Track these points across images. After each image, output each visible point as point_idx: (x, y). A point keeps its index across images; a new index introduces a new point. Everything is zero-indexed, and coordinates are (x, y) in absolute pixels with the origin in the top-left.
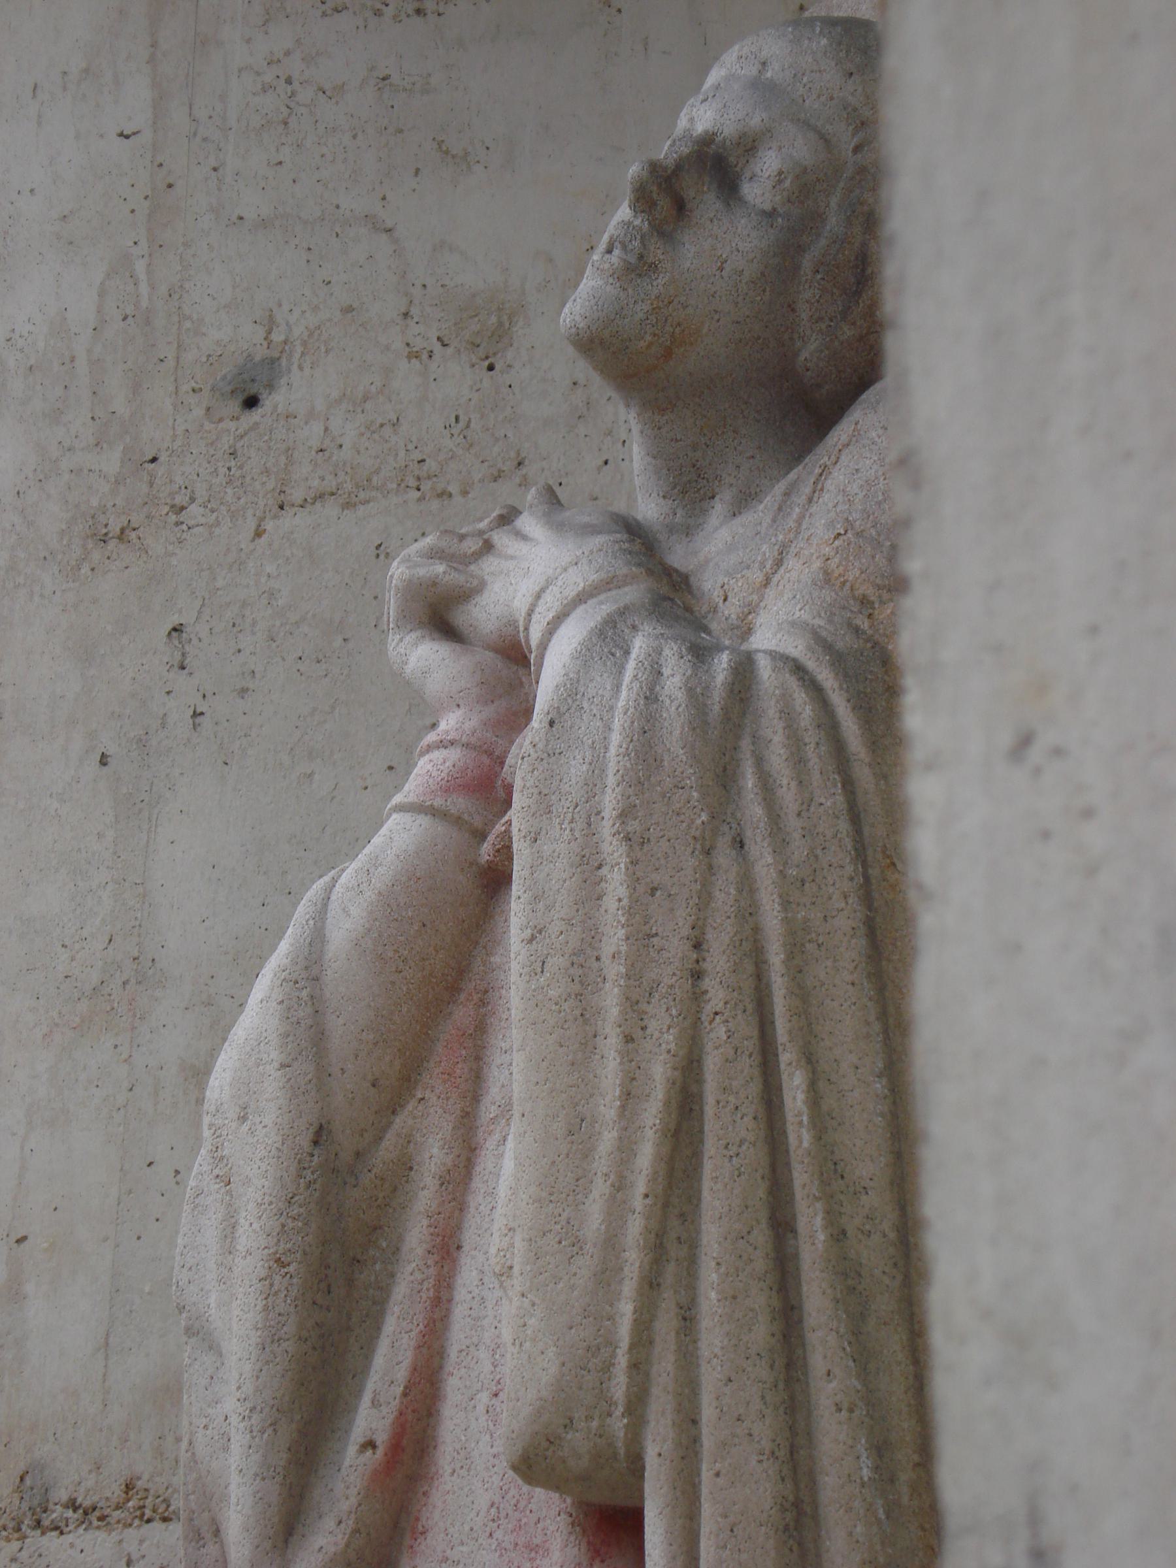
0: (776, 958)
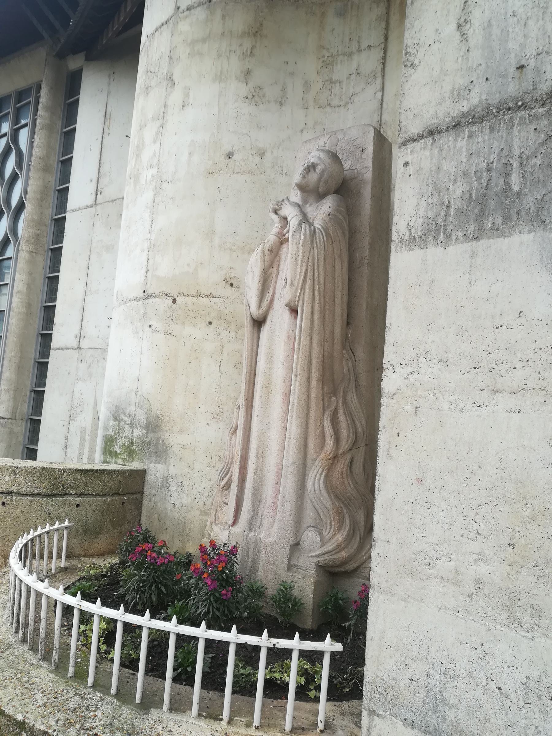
0: (316, 261)
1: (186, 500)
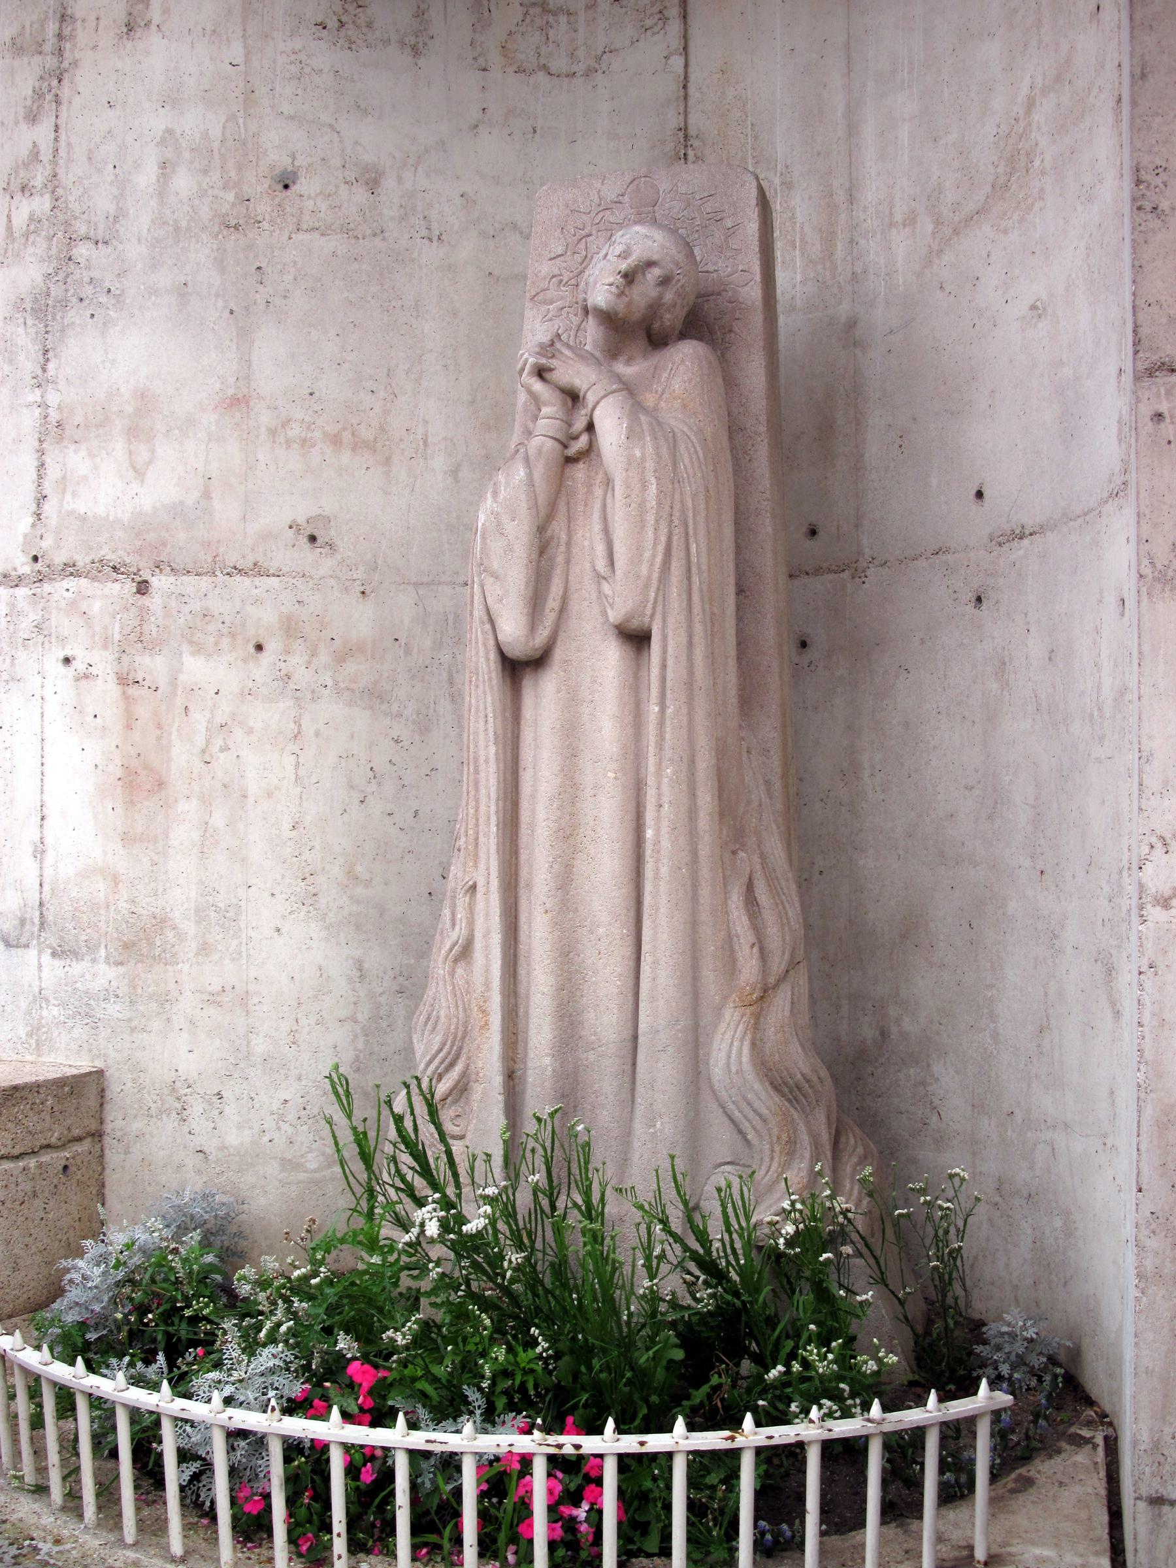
1: (235, 1138)
